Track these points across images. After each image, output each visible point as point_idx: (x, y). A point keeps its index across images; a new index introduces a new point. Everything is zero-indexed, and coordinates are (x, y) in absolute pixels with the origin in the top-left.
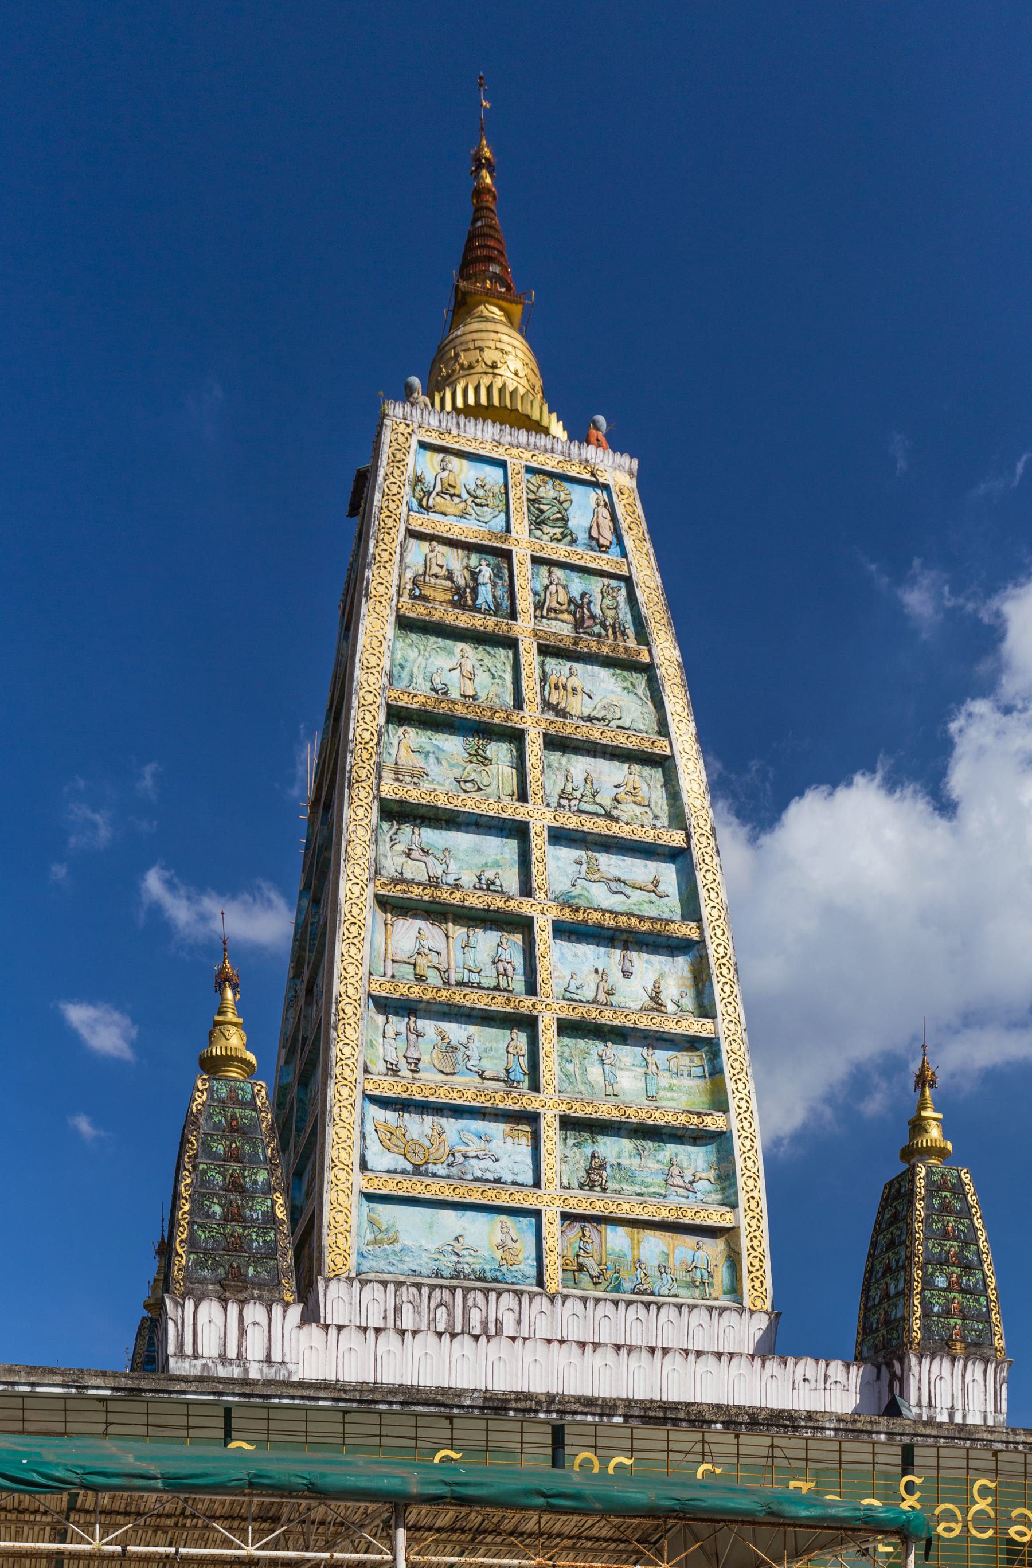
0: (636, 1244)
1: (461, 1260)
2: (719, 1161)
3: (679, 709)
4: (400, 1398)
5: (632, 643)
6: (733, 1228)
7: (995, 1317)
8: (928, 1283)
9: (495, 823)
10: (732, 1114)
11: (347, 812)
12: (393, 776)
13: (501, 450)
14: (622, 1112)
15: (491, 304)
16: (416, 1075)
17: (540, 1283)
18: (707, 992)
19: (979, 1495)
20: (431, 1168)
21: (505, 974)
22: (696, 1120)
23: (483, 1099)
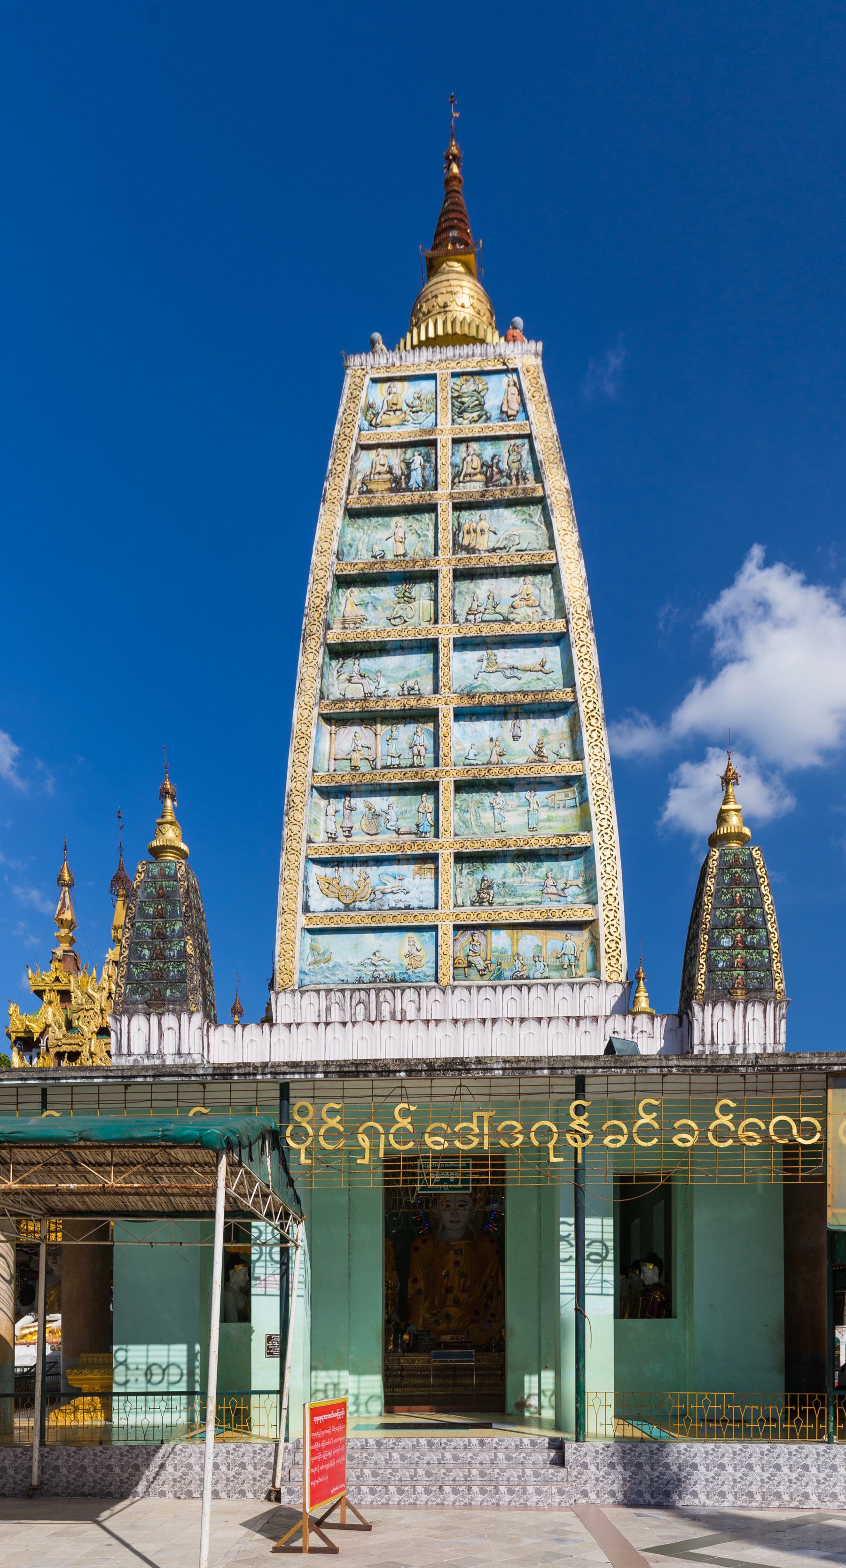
0: (515, 942)
1: (378, 968)
2: (586, 869)
3: (565, 525)
4: (151, 1073)
5: (531, 484)
6: (594, 920)
7: (776, 966)
8: (713, 944)
9: (414, 644)
10: (595, 831)
11: (301, 659)
12: (341, 626)
13: (433, 366)
14: (504, 843)
15: (450, 260)
16: (350, 839)
17: (437, 980)
18: (578, 740)
19: (721, 1111)
20: (358, 904)
21: (419, 755)
22: (564, 841)
23: (395, 849)
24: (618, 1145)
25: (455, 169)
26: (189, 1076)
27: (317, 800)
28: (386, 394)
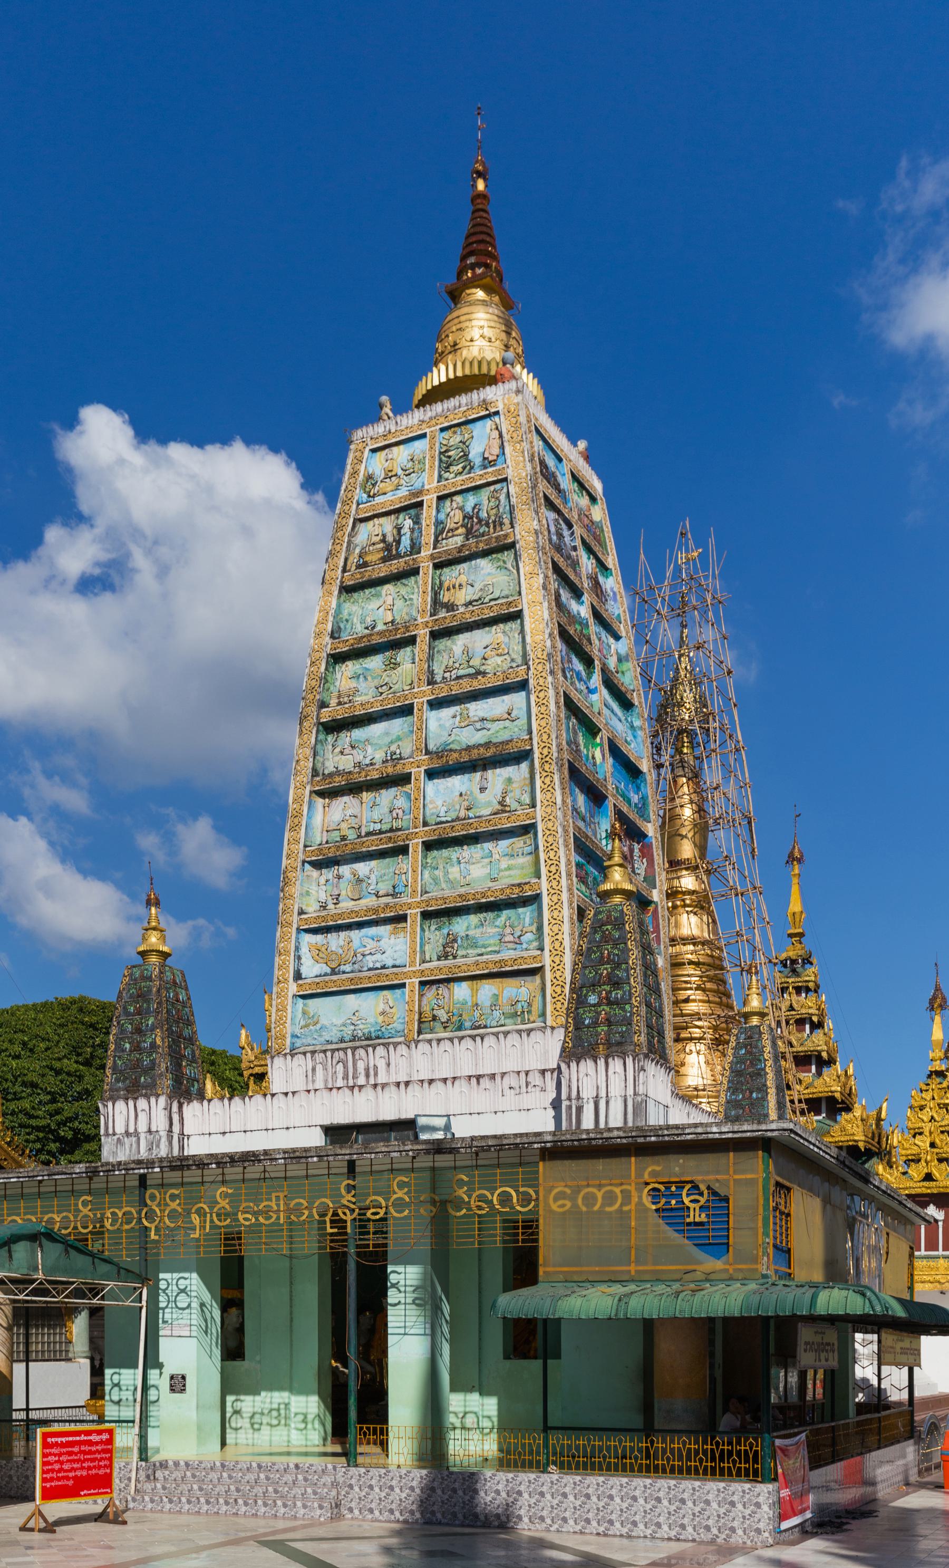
0: (475, 992)
15: (468, 288)
20: (342, 968)
22: (516, 890)
24: (377, 1217)
25: (481, 185)
26: (71, 1174)
27: (309, 873)
28: (384, 462)
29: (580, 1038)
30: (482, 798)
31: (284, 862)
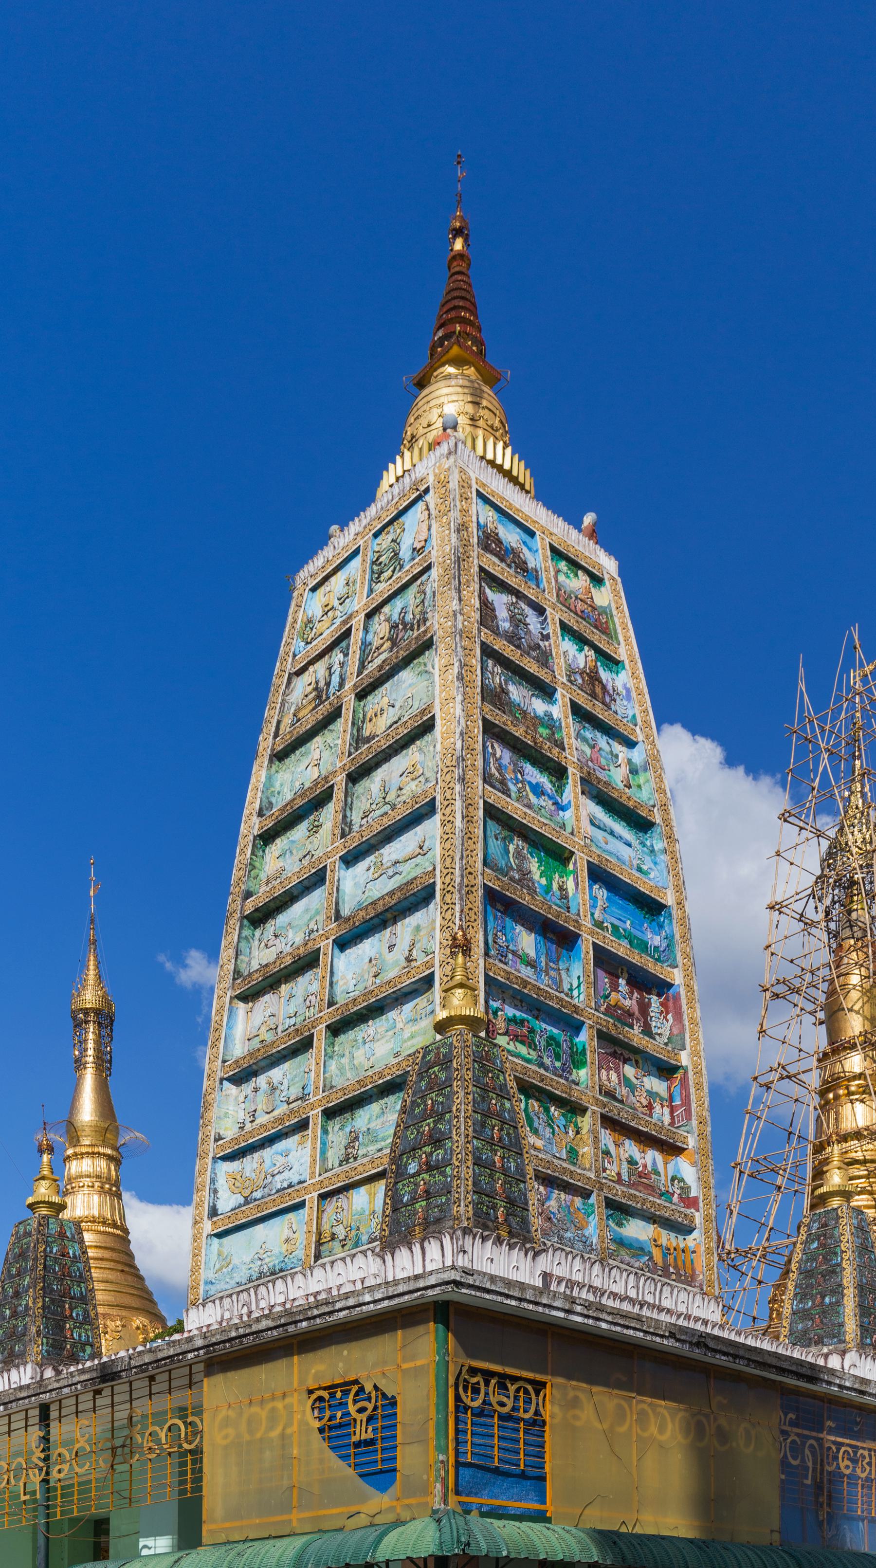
15: (435, 370)
29: (399, 1223)
30: (390, 958)
31: (205, 1084)
